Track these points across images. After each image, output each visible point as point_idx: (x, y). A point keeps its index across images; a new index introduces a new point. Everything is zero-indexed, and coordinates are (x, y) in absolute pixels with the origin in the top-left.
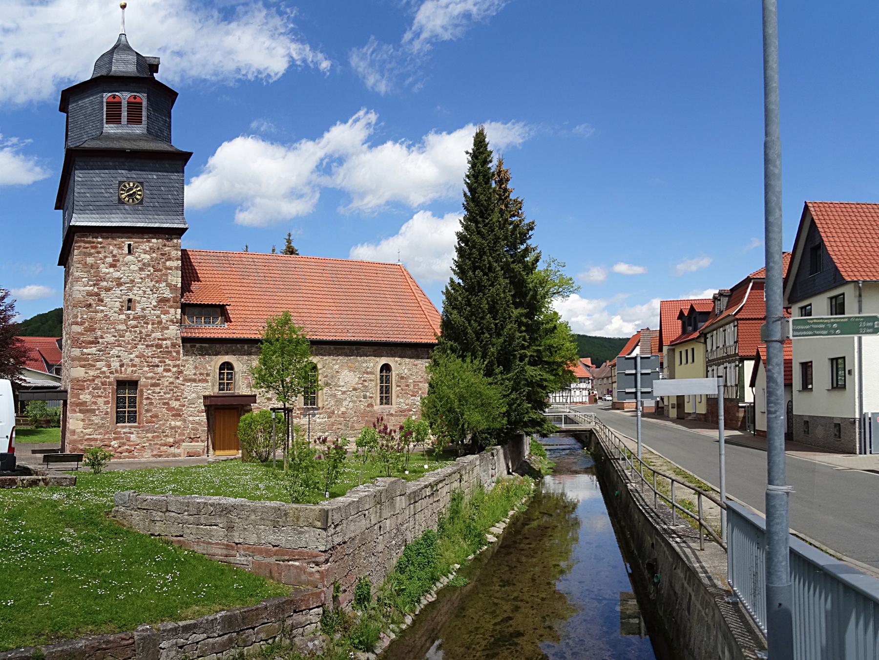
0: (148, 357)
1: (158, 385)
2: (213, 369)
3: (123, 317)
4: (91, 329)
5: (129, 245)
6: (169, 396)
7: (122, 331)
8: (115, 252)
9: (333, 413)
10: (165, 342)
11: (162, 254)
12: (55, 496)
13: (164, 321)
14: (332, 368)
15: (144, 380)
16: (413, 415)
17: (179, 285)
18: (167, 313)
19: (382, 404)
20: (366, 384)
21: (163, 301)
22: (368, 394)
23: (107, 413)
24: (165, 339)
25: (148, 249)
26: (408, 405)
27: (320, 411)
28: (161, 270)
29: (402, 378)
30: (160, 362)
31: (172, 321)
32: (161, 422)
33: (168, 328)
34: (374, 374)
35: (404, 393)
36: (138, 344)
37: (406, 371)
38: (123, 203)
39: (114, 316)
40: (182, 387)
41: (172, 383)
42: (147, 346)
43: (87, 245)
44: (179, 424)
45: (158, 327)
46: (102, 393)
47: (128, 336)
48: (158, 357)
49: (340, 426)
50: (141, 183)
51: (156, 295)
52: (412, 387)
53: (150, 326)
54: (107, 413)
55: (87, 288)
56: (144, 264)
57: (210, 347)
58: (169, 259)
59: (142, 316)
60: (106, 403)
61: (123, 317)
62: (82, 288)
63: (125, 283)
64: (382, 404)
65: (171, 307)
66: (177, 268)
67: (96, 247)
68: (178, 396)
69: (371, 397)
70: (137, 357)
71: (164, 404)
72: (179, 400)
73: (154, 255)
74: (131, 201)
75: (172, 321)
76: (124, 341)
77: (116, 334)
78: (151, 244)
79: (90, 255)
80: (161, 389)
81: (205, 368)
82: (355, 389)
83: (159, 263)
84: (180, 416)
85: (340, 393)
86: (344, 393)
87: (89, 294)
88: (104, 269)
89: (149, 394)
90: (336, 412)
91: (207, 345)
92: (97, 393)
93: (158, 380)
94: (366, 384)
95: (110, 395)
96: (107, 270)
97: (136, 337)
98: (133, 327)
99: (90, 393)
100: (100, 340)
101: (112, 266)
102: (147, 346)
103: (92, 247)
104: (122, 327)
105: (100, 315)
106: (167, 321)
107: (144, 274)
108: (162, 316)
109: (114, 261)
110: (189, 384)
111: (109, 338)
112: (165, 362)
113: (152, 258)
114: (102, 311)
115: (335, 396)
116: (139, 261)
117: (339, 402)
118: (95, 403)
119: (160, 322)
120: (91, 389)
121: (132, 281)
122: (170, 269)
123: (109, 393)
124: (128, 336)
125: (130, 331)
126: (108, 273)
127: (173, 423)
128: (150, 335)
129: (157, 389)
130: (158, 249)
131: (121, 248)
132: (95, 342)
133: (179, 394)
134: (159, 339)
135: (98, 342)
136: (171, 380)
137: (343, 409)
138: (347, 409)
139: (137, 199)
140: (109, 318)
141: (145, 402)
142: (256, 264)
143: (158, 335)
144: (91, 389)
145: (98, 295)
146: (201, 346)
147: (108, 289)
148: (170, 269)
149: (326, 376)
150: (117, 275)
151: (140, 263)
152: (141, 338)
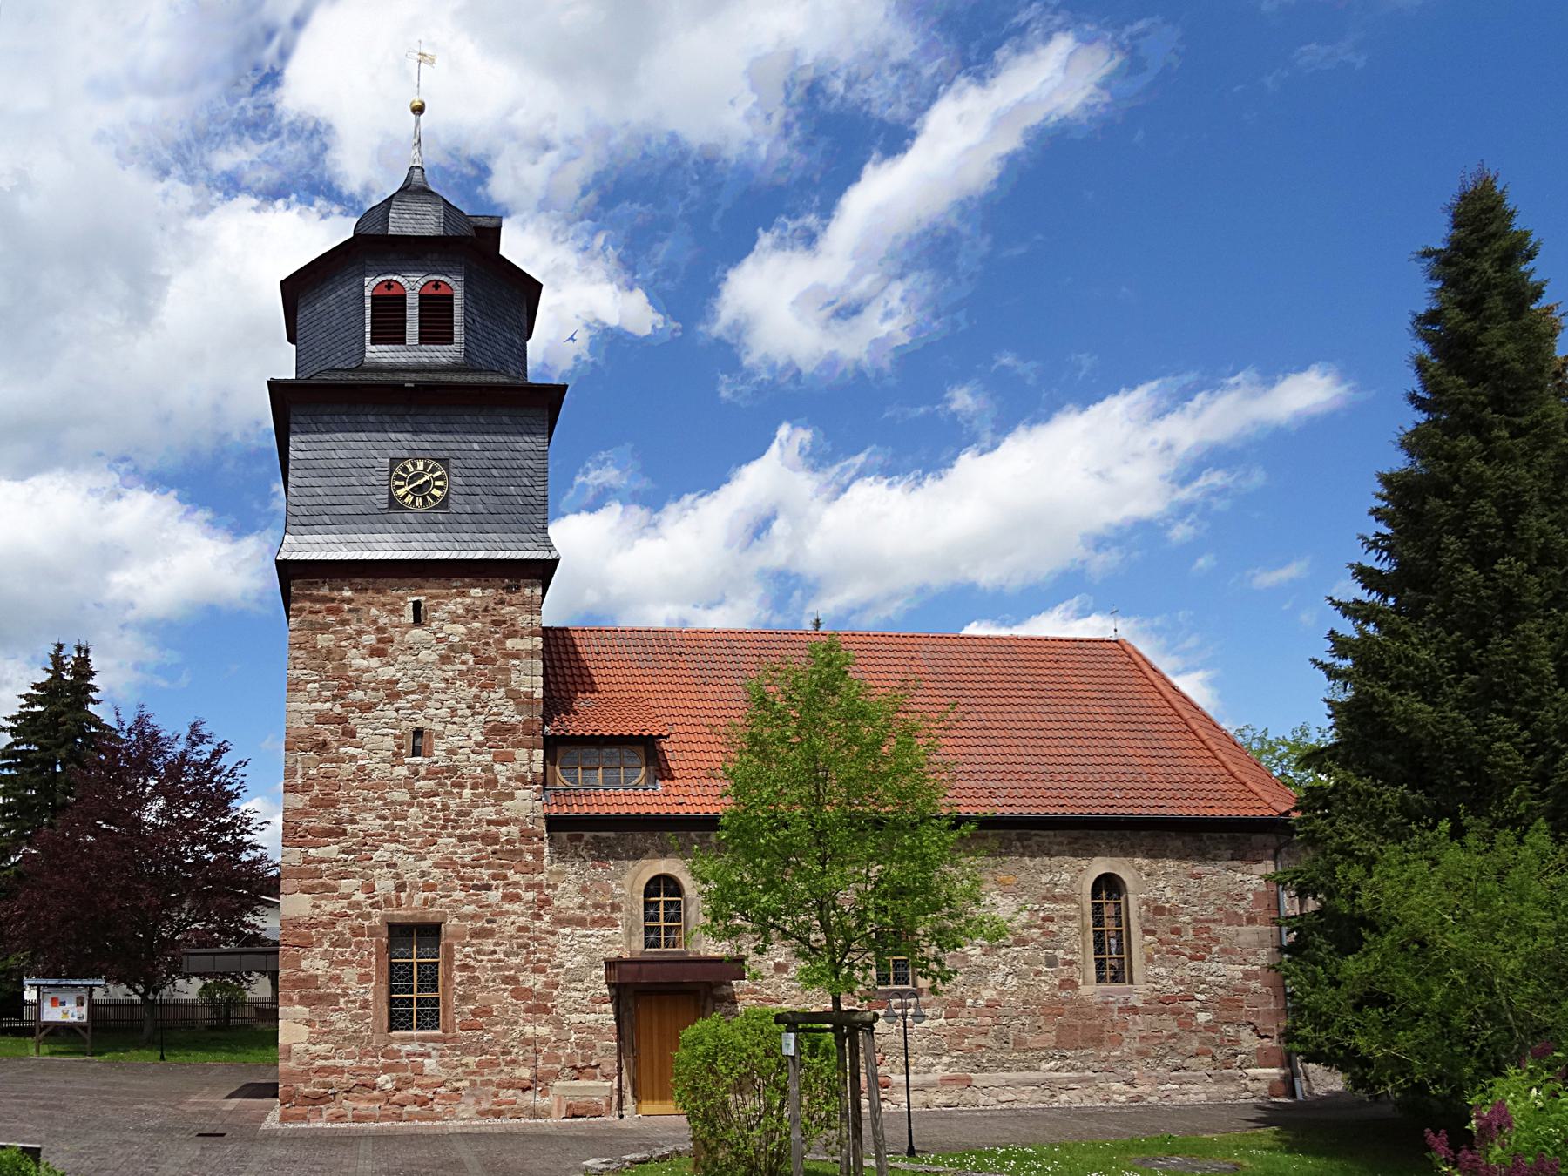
0: (464, 866)
1: (489, 934)
2: (627, 892)
3: (402, 771)
4: (328, 802)
5: (417, 605)
8: (382, 621)
10: (504, 829)
13: (502, 779)
15: (455, 921)
18: (508, 759)
20: (1053, 927)
21: (497, 731)
22: (1060, 954)
24: (506, 823)
25: (460, 611)
26: (1182, 982)
28: (493, 661)
29: (1159, 910)
30: (495, 877)
32: (498, 1028)
33: (511, 796)
35: (1168, 951)
36: (438, 835)
37: (1169, 893)
38: (401, 508)
39: (380, 770)
40: (551, 939)
42: (462, 839)
43: (318, 606)
44: (543, 1031)
48: (489, 866)
49: (982, 1040)
52: (1189, 935)
53: (467, 792)
54: (365, 1005)
55: (318, 705)
56: (451, 648)
58: (513, 634)
60: (364, 979)
61: (402, 771)
62: (306, 706)
63: (406, 693)
65: (518, 745)
66: (531, 654)
68: (539, 961)
69: (1070, 963)
70: (436, 865)
71: (506, 980)
72: (543, 971)
73: (476, 625)
75: (521, 778)
76: (405, 829)
77: (386, 813)
78: (468, 601)
79: (325, 628)
80: (497, 944)
81: (609, 891)
83: (487, 644)
84: (548, 1011)
87: (324, 719)
88: (356, 660)
90: (969, 1002)
92: (342, 954)
93: (489, 921)
94: (1053, 927)
95: (373, 959)
97: (433, 818)
98: (427, 795)
100: (349, 828)
101: (376, 652)
102: (462, 839)
103: (330, 611)
104: (401, 795)
105: (348, 768)
106: (509, 779)
108: (497, 767)
109: (379, 641)
110: (568, 931)
111: (370, 822)
112: (505, 877)
113: (471, 631)
114: (353, 758)
116: (439, 640)
118: (337, 980)
119: (492, 783)
120: (326, 945)
122: (516, 656)
123: (370, 954)
125: (421, 805)
126: (368, 670)
127: (529, 1029)
128: (468, 814)
129: (488, 944)
130: (486, 610)
132: (337, 832)
133: (543, 956)
134: (489, 823)
135: (344, 833)
136: (522, 921)
137: (989, 994)
138: (1001, 993)
139: (434, 498)
140: (369, 775)
141: (458, 976)
143: (488, 812)
144: (326, 945)
146: (595, 837)
147: (367, 708)
148: (516, 656)
150: (387, 673)
152: (446, 820)
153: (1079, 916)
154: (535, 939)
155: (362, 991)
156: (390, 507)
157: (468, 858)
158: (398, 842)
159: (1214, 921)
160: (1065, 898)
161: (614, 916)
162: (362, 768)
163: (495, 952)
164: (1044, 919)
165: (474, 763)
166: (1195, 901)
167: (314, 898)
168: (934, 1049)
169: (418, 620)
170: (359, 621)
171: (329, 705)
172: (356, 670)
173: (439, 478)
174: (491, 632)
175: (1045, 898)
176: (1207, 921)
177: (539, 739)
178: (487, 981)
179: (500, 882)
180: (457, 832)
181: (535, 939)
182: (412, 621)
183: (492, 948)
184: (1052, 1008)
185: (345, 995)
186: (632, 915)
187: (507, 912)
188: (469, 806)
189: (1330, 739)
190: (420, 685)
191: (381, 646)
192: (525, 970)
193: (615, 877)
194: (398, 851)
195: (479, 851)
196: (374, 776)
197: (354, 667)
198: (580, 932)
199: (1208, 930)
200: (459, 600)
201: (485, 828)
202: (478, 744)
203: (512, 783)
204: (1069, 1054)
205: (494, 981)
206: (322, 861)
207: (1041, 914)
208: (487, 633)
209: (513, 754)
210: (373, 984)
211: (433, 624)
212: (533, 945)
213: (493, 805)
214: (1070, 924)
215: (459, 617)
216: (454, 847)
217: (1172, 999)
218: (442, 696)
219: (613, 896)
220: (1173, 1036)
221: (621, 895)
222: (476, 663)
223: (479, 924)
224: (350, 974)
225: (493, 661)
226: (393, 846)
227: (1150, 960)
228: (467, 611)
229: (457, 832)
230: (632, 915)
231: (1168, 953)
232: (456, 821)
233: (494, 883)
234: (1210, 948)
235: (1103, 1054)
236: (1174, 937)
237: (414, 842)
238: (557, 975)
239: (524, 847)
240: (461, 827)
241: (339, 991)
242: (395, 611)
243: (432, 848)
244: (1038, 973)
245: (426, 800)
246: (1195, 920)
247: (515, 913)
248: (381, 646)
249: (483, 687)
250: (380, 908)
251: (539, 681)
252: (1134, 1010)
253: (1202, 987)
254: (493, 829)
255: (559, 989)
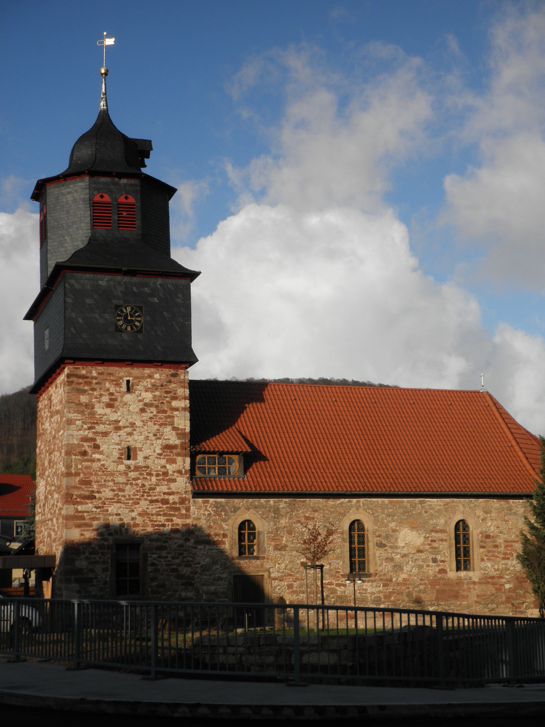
0: (152, 515)
1: (165, 548)
2: (230, 528)
3: (122, 468)
4: (88, 483)
5: (128, 382)
6: (177, 561)
7: (122, 483)
8: (112, 390)
9: (391, 580)
10: (171, 497)
11: (167, 392)
12: (86, 388)
13: (170, 472)
14: (387, 526)
15: (148, 542)
16: (505, 583)
17: (188, 430)
18: (173, 461)
19: (458, 569)
20: (435, 545)
21: (168, 447)
22: (439, 557)
23: (105, 583)
24: (172, 493)
25: (149, 386)
26: (498, 570)
27: (372, 578)
28: (165, 412)
29: (488, 537)
30: (168, 520)
31: (180, 472)
32: (169, 593)
33: (174, 481)
34: (446, 532)
35: (491, 556)
36: (140, 499)
37: (492, 529)
38: (121, 331)
39: (111, 467)
40: (194, 551)
41: (181, 546)
42: (152, 501)
43: (81, 380)
44: (190, 594)
45: (164, 480)
46: (100, 558)
47: (129, 490)
48: (165, 515)
49: (400, 597)
50: (140, 308)
51: (160, 441)
52: (502, 549)
53: (154, 479)
54: (105, 583)
55: (81, 432)
56: (146, 405)
57: (226, 503)
58: (175, 398)
59: (145, 467)
60: (105, 570)
61: (122, 468)
62: (75, 433)
63: (124, 427)
64: (458, 569)
65: (178, 455)
66: (184, 409)
67: (89, 383)
68: (188, 561)
69: (443, 561)
70: (140, 514)
71: (173, 570)
72: (190, 566)
73: (157, 393)
74: (129, 328)
75: (180, 472)
76: (124, 496)
77: (115, 488)
78: (153, 381)
79: (84, 392)
80: (168, 553)
81: (221, 528)
82: (419, 551)
83: (163, 403)
84: (192, 585)
85: (399, 556)
86: (404, 556)
87: (85, 439)
88: (100, 410)
89: (154, 559)
90: (394, 580)
91: (223, 500)
92: (94, 558)
93: (165, 542)
94: (435, 545)
95: (109, 561)
96: (103, 412)
97: (137, 491)
98: (135, 479)
99: (87, 558)
100: (97, 495)
101: (109, 406)
102: (152, 501)
103: (86, 383)
104: (121, 479)
105: (96, 465)
106: (174, 472)
107: (146, 416)
108: (168, 466)
109: (111, 399)
110: (202, 547)
111: (107, 493)
112: (172, 521)
113: (155, 396)
114: (99, 460)
115: (392, 559)
116: (140, 401)
117: (398, 568)
118: (92, 571)
119: (166, 474)
120: (87, 554)
121: (132, 425)
122: (177, 409)
123: (108, 558)
124: (129, 490)
125: (131, 484)
126: (105, 415)
127: (183, 594)
128: (154, 489)
129: (164, 553)
130: (162, 386)
131: (118, 385)
132: (91, 497)
133: (190, 559)
134: (165, 493)
135: (95, 498)
136: (181, 542)
137: (403, 576)
138: (410, 575)
139: (136, 326)
140: (106, 469)
141: (150, 569)
142: (311, 484)
143: (164, 489)
144: (87, 554)
145: (94, 440)
146: (216, 502)
147: (105, 434)
148: (177, 409)
149: (379, 536)
150: (114, 417)
151: (141, 403)
152: (144, 492)
153: (448, 539)
154: (186, 550)
155: (104, 576)
156: (116, 331)
157: (154, 512)
158: (121, 502)
159: (515, 542)
160: (442, 531)
161: (224, 540)
162: (103, 465)
163: (167, 557)
164: (432, 541)
165: (157, 464)
166: (506, 532)
167: (81, 530)
168: (376, 601)
169: (129, 390)
170: (101, 389)
171: (86, 432)
172: (99, 415)
173: (139, 316)
174: (165, 397)
175: (432, 531)
176: (511, 541)
177: (188, 452)
178: (163, 571)
179: (170, 523)
180: (149, 498)
181: (186, 550)
182: (126, 390)
183: (166, 555)
184: (434, 582)
185: (96, 578)
186: (232, 539)
187: (173, 538)
188: (155, 485)
189: (300, 609)
190: (130, 424)
191: (112, 402)
192: (181, 565)
193: (224, 520)
194: (120, 507)
195: (160, 508)
196: (109, 470)
197: (98, 413)
198: (207, 547)
199: (511, 546)
200: (148, 380)
201: (162, 497)
202: (159, 454)
203: (175, 474)
204: (442, 603)
205: (167, 571)
206: (83, 512)
207: (430, 539)
208: (163, 398)
209: (175, 459)
210: (109, 573)
211: (137, 392)
212: (186, 554)
213: (166, 485)
214: (444, 543)
215: (149, 388)
216: (148, 505)
217: (493, 578)
218: (142, 429)
219: (223, 530)
220: (493, 595)
221: (228, 530)
222: (158, 412)
223: (160, 544)
224: (98, 568)
225: (165, 412)
226: (119, 505)
227: (482, 560)
228: (153, 385)
229: (149, 498)
230: (232, 539)
231: (491, 556)
232: (148, 493)
233: (167, 523)
234: (512, 554)
235: (458, 603)
236: (495, 549)
237: (128, 503)
238: (197, 568)
239: (181, 506)
240: (150, 496)
241: (93, 576)
242: (118, 385)
243: (137, 506)
244: (428, 566)
245: (134, 482)
246: (506, 541)
247: (176, 538)
248: (112, 402)
249: (161, 425)
250: (113, 536)
251: (188, 423)
252: (474, 583)
253: (508, 572)
254: (166, 497)
255: (198, 575)
